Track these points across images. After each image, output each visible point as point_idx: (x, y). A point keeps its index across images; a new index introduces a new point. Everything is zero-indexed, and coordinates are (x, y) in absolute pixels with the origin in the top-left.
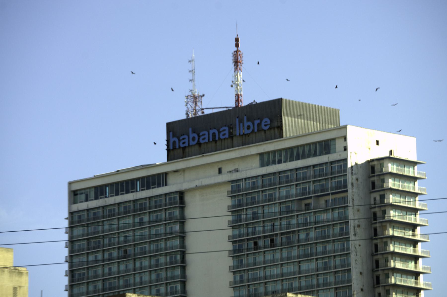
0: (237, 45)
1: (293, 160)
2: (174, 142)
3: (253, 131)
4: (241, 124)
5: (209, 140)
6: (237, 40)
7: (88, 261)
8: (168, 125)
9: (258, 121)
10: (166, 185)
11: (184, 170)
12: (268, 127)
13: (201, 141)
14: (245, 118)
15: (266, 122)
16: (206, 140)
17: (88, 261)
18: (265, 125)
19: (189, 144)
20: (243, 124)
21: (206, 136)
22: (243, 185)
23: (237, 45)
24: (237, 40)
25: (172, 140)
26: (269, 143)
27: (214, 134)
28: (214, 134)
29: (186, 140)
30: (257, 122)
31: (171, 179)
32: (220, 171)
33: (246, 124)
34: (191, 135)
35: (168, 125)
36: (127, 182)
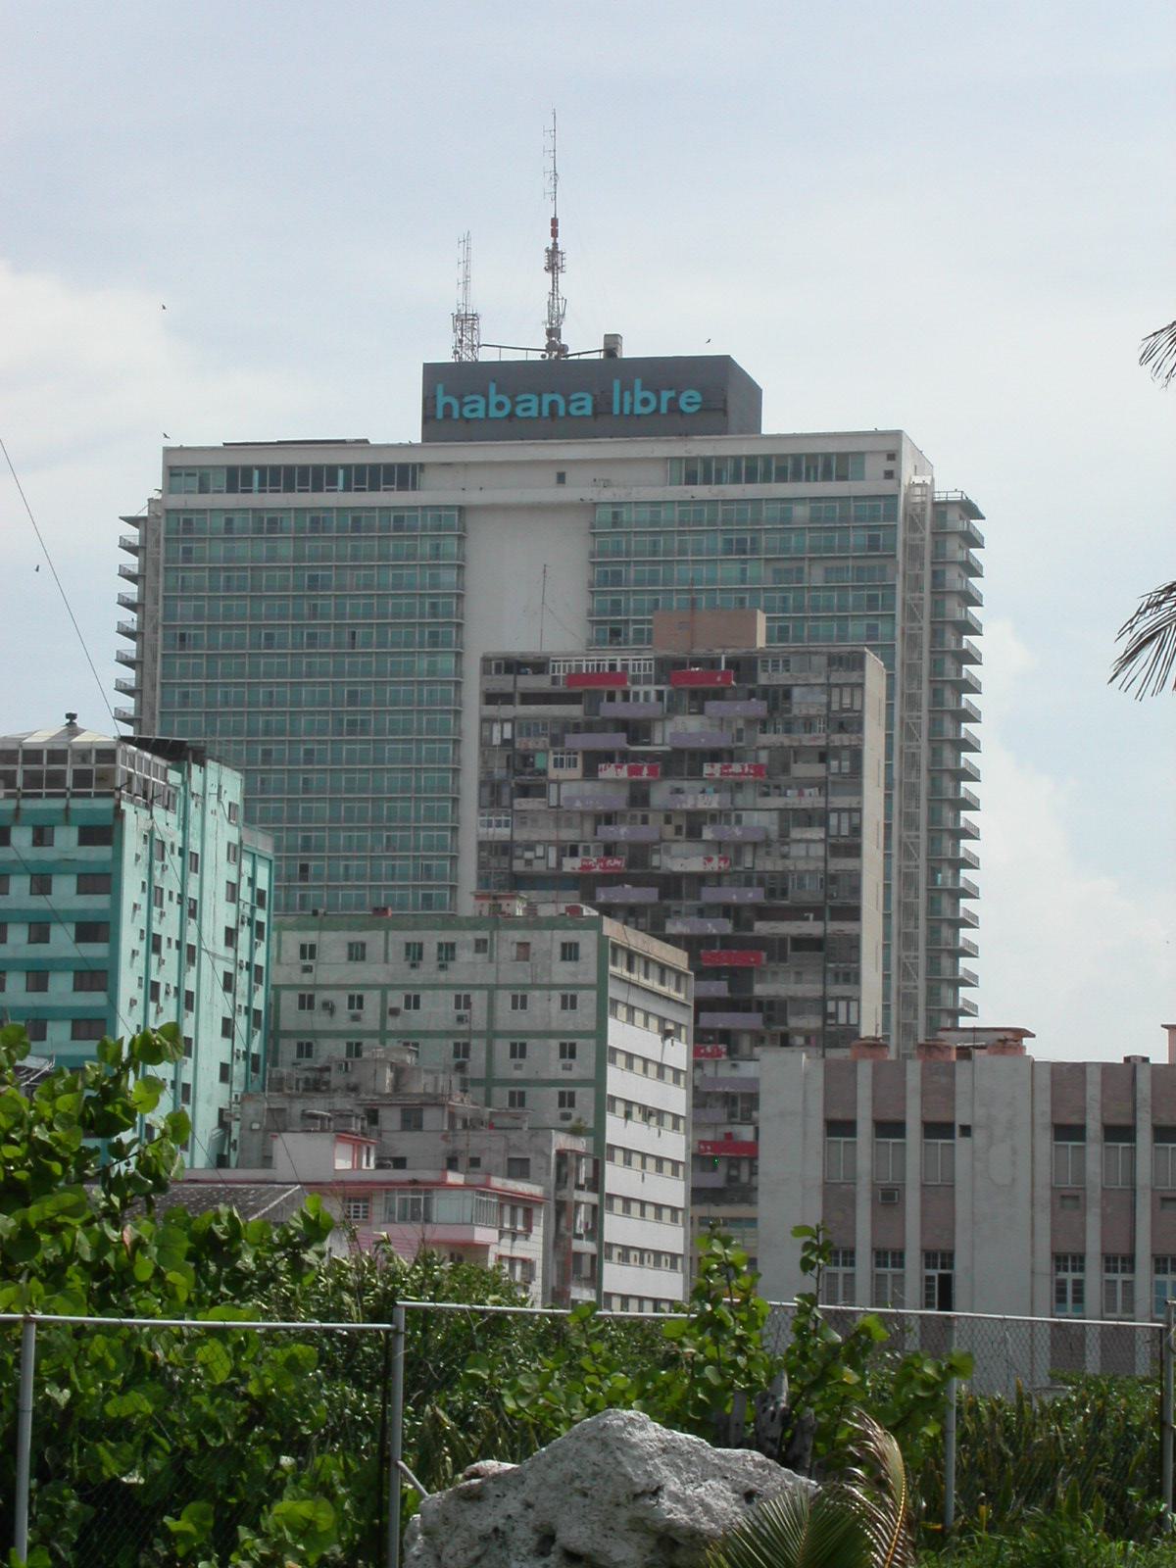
0: (554, 233)
1: (830, 479)
2: (448, 407)
3: (657, 410)
4: (627, 395)
5: (540, 413)
6: (554, 222)
7: (808, 856)
8: (606, 336)
9: (672, 394)
10: (414, 488)
11: (466, 465)
12: (697, 407)
13: (519, 412)
14: (638, 383)
15: (691, 397)
16: (534, 413)
17: (808, 856)
18: (689, 404)
19: (487, 415)
20: (632, 395)
21: (534, 405)
22: (664, 514)
23: (554, 233)
24: (554, 222)
25: (442, 400)
26: (579, 443)
27: (553, 405)
28: (553, 405)
29: (481, 406)
30: (666, 395)
31: (427, 478)
32: (561, 478)
33: (640, 395)
34: (494, 399)
35: (606, 336)
36: (318, 469)
